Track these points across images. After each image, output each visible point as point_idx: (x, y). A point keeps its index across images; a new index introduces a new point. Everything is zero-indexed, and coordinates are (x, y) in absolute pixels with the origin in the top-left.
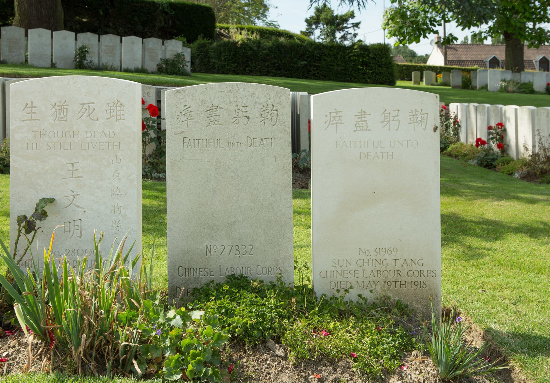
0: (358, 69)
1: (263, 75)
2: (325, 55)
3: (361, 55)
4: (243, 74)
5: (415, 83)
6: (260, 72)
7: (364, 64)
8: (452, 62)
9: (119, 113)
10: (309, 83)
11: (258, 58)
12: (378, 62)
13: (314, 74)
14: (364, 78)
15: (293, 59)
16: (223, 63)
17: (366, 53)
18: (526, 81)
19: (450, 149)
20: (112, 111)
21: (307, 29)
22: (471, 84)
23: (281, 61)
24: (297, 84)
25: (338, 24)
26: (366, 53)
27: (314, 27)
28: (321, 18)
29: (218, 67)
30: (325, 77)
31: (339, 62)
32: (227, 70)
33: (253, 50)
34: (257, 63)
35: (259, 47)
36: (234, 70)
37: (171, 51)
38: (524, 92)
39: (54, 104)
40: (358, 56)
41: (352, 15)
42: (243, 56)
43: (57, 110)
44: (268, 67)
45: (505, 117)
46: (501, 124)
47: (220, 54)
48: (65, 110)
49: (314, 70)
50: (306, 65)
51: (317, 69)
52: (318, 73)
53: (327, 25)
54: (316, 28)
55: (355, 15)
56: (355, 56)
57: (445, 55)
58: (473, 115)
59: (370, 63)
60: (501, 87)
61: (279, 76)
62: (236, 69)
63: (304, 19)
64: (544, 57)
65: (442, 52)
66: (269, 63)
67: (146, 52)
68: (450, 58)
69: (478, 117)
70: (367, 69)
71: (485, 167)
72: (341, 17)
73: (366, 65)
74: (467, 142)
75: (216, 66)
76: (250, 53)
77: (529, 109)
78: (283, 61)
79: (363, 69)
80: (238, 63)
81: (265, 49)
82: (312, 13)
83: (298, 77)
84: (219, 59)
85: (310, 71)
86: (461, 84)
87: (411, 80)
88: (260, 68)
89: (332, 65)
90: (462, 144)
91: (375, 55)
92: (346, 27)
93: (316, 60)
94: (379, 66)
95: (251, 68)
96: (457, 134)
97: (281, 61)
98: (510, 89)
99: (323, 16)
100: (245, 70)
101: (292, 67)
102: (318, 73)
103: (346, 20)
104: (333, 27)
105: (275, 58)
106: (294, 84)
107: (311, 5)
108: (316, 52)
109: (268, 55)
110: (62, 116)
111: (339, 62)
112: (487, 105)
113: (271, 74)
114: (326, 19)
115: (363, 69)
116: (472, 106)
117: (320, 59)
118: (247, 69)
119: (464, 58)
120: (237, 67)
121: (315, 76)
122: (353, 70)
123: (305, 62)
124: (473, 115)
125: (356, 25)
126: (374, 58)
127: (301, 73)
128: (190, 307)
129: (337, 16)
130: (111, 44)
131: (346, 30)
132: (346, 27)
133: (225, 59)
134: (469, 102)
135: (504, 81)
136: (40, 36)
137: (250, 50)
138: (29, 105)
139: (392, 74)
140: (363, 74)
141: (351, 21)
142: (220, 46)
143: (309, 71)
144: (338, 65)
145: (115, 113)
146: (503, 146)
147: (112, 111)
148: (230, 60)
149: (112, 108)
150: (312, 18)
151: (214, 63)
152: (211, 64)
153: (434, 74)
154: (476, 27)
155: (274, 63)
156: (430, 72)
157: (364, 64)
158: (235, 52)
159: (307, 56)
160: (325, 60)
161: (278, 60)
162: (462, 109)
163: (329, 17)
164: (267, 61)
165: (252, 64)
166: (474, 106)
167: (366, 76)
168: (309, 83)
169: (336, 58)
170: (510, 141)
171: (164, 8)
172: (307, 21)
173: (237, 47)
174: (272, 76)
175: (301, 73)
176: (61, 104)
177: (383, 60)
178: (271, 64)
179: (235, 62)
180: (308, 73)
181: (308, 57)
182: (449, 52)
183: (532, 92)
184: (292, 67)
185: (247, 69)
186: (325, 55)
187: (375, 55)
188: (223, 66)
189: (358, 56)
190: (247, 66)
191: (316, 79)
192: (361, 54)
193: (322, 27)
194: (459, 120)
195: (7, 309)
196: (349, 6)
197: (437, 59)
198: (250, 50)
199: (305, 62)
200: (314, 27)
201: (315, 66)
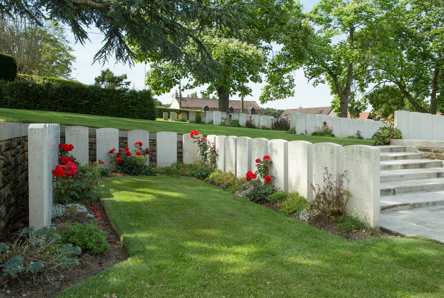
0: (129, 108)
1: (52, 110)
2: (104, 96)
3: (131, 97)
4: (34, 109)
5: (164, 119)
6: (49, 108)
7: (133, 104)
8: (184, 108)
10: (87, 117)
11: (48, 97)
12: (143, 103)
13: (95, 111)
14: (133, 115)
15: (77, 98)
16: (15, 100)
17: (135, 96)
18: (235, 119)
19: (211, 176)
21: (95, 84)
22: (201, 120)
23: (68, 100)
24: (76, 118)
25: (117, 82)
26: (135, 96)
27: (101, 83)
28: (105, 77)
29: (10, 103)
30: (103, 113)
31: (115, 102)
32: (19, 105)
33: (43, 90)
34: (47, 100)
35: (48, 88)
36: (25, 106)
38: (234, 126)
40: (129, 98)
41: (125, 77)
42: (34, 95)
44: (56, 104)
45: (272, 150)
46: (267, 157)
47: (13, 92)
49: (95, 108)
50: (88, 103)
51: (97, 107)
52: (98, 110)
54: (102, 84)
55: (127, 77)
56: (126, 98)
57: (180, 104)
58: (232, 147)
59: (138, 103)
60: (221, 123)
61: (65, 112)
62: (27, 105)
63: (95, 78)
65: (178, 102)
66: (57, 101)
68: (183, 106)
69: (238, 148)
70: (135, 108)
71: (257, 202)
72: (118, 78)
73: (135, 105)
74: (225, 170)
75: (9, 102)
76: (40, 92)
77: (304, 144)
78: (69, 100)
79: (132, 108)
80: (30, 100)
81: (53, 90)
82: (99, 74)
83: (82, 113)
84: (12, 96)
85: (92, 108)
86: (195, 120)
87: (162, 118)
88: (50, 105)
89: (109, 104)
90: (220, 171)
91: (142, 98)
92: (121, 84)
93: (96, 100)
94: (145, 106)
95: (41, 104)
96: (214, 161)
97: (68, 100)
98: (227, 124)
99: (106, 76)
100: (35, 106)
101: (77, 105)
102: (98, 110)
103: (121, 80)
104: (113, 84)
105: (63, 97)
106: (74, 117)
107: (95, 61)
108: (96, 94)
109: (56, 95)
111: (115, 102)
112: (248, 138)
113: (59, 110)
114: (108, 78)
115: (132, 108)
116: (231, 138)
117: (99, 100)
118: (37, 105)
119: (190, 106)
120: (28, 103)
121: (96, 112)
122: (125, 108)
123: (88, 101)
124: (232, 146)
125: (128, 83)
126: (140, 100)
127: (84, 110)
129: (115, 77)
131: (122, 86)
132: (121, 84)
133: (17, 96)
134: (227, 135)
135: (222, 119)
137: (41, 90)
139: (153, 112)
140: (133, 111)
141: (125, 81)
142: (12, 86)
143: (90, 108)
144: (113, 104)
146: (269, 180)
148: (22, 98)
150: (99, 77)
151: (7, 99)
152: (4, 100)
153: (176, 114)
155: (62, 102)
156: (174, 113)
157: (133, 104)
158: (27, 91)
159: (89, 96)
160: (103, 100)
161: (65, 99)
162: (220, 141)
163: (110, 77)
164: (56, 99)
165: (42, 101)
166: (233, 138)
167: (135, 113)
168: (87, 117)
169: (112, 99)
170: (277, 173)
172: (96, 79)
173: (29, 87)
174: (60, 111)
175: (84, 110)
177: (147, 101)
178: (59, 102)
179: (26, 100)
180: (90, 110)
181: (90, 98)
182: (182, 102)
183: (239, 126)
184: (77, 105)
185: (37, 105)
186: (104, 96)
187: (142, 98)
188: (15, 103)
189: (129, 98)
190: (38, 103)
191: (96, 115)
192: (131, 96)
193: (106, 83)
194: (216, 150)
196: (123, 64)
197: (176, 105)
198: (41, 90)
199: (88, 101)
200: (101, 83)
201: (95, 105)
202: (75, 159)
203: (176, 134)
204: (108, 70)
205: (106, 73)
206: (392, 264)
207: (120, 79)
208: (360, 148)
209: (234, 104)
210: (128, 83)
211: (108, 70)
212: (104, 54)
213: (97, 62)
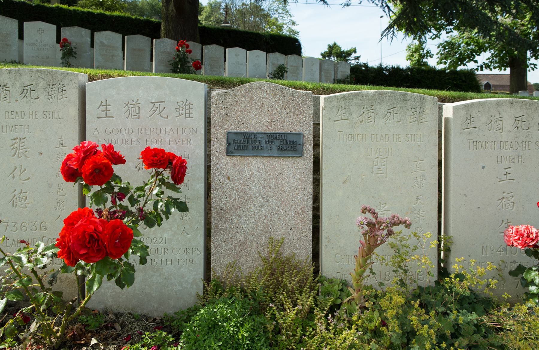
9: (187, 111)
20: (181, 109)
25: (345, 57)
37: (342, 72)
39: (127, 103)
43: (130, 108)
48: (137, 108)
53: (337, 58)
55: (357, 51)
63: (320, 53)
64: (488, 83)
67: (322, 73)
72: (347, 52)
92: (349, 60)
99: (334, 51)
110: (134, 114)
114: (336, 53)
125: (357, 58)
128: (92, 227)
129: (343, 51)
130: (295, 65)
136: (237, 55)
138: (104, 103)
141: (354, 55)
145: (184, 111)
147: (181, 109)
149: (181, 106)
150: (326, 52)
154: (61, 56)
171: (266, 39)
176: (134, 103)
195: (195, 312)
202: (198, 295)
203: (55, 26)
204: (335, 44)
205: (333, 47)
206: (313, 329)
207: (349, 54)
208: (405, 95)
209: (490, 79)
210: (357, 58)
211: (335, 44)
212: (392, 29)
213: (385, 38)
